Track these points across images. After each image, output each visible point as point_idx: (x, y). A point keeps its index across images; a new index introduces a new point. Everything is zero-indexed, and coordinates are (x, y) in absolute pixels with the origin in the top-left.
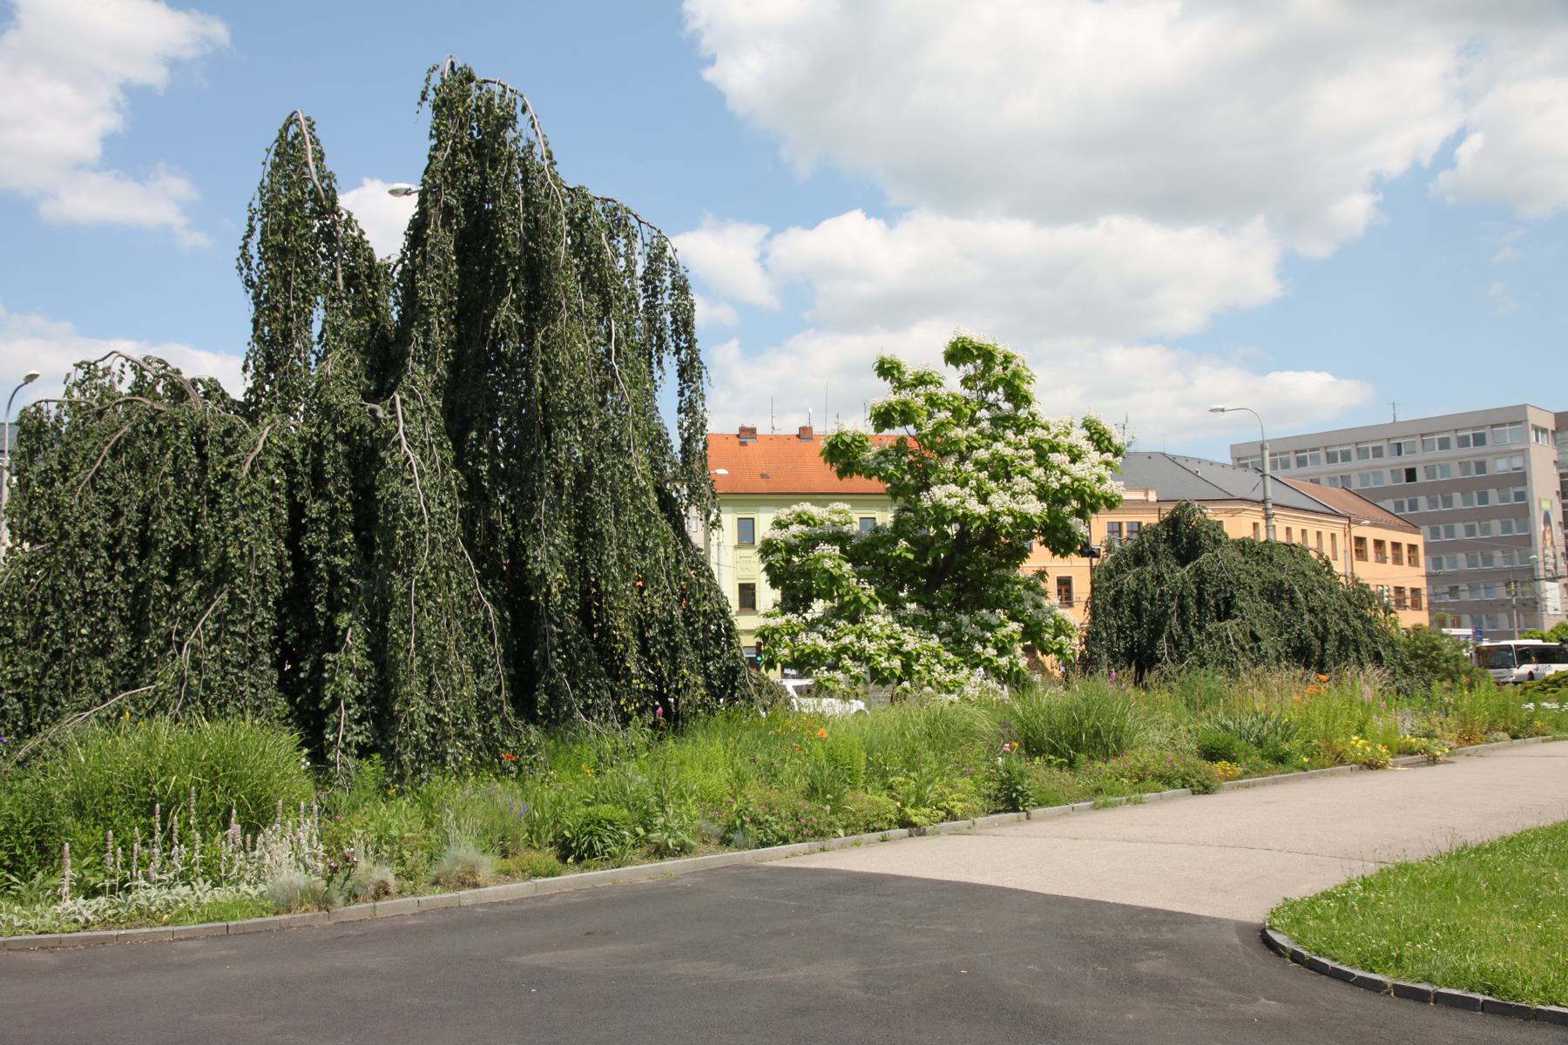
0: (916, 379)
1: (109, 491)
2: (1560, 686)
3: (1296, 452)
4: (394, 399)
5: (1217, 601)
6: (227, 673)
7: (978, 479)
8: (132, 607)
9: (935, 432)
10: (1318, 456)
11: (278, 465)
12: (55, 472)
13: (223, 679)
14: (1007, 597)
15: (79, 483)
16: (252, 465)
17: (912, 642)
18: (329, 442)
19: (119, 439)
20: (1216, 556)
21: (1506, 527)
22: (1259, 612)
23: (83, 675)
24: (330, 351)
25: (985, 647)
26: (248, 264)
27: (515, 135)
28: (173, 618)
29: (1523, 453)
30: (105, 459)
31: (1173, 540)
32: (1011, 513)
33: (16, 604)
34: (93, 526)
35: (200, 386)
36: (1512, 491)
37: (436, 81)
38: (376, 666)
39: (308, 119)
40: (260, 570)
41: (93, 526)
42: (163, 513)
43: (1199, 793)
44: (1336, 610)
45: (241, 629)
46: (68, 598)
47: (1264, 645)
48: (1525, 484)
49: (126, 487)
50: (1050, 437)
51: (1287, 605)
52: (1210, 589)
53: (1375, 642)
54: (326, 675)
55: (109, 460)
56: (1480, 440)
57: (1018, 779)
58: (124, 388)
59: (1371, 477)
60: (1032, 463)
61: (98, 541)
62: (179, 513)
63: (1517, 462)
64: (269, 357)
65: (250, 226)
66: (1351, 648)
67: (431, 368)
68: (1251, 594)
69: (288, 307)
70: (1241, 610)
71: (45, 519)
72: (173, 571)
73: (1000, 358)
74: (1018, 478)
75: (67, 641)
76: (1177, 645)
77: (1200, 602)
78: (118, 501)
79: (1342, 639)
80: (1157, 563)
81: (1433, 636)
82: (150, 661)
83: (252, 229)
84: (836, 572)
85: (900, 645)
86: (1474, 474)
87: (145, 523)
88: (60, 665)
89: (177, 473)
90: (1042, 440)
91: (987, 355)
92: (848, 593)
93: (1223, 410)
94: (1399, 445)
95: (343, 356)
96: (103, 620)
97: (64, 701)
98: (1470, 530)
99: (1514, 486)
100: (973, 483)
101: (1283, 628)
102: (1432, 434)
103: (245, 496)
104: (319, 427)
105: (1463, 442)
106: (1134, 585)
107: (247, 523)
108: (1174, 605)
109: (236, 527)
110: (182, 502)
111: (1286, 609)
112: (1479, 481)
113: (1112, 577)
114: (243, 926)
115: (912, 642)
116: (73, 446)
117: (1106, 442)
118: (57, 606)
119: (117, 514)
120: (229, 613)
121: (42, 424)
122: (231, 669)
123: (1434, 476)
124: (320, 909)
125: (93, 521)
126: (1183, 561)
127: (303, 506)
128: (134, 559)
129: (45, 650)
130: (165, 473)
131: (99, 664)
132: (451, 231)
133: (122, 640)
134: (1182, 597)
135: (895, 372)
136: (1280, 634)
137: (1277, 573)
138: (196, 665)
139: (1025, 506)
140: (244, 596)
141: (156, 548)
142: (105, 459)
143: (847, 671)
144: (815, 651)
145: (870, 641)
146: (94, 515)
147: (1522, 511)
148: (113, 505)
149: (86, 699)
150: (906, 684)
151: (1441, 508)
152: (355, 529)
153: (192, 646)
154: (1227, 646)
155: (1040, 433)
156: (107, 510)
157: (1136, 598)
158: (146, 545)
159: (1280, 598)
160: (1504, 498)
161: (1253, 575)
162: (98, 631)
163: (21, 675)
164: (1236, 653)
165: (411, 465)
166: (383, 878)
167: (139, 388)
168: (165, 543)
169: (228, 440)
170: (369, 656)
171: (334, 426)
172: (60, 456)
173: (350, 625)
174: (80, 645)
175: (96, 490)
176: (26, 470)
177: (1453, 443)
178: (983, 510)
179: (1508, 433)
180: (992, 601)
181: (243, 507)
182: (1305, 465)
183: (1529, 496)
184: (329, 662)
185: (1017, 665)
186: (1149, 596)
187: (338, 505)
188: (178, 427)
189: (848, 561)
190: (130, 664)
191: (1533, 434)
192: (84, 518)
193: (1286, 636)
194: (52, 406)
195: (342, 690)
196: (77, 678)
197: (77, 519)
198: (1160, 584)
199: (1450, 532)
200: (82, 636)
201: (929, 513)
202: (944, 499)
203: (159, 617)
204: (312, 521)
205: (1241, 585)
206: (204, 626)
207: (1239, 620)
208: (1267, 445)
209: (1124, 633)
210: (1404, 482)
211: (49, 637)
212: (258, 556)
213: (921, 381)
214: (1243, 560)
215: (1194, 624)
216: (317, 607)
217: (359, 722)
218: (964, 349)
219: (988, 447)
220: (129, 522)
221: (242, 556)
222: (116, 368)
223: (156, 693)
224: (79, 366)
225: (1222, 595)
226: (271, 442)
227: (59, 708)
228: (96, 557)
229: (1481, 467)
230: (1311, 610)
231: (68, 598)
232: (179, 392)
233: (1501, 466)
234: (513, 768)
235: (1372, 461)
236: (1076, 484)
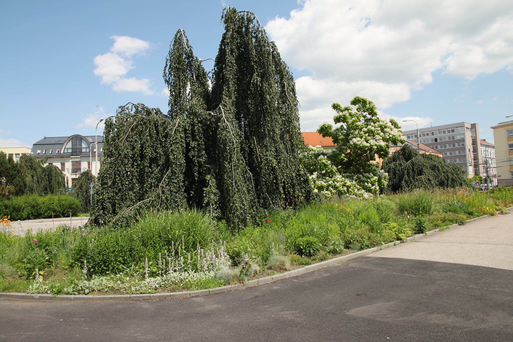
0: (345, 109)
1: (131, 142)
3: (407, 135)
4: (220, 107)
6: (172, 195)
7: (365, 136)
8: (139, 175)
9: (353, 123)
10: (413, 136)
11: (182, 131)
12: (116, 137)
13: (171, 197)
14: (371, 170)
15: (123, 139)
16: (175, 132)
17: (348, 183)
18: (196, 123)
19: (133, 126)
20: (417, 158)
22: (430, 173)
23: (127, 196)
24: (193, 98)
25: (368, 184)
26: (166, 75)
27: (253, 26)
28: (152, 178)
29: (464, 134)
30: (129, 132)
31: (404, 154)
32: (376, 145)
33: (108, 175)
34: (128, 152)
35: (154, 110)
36: (461, 144)
37: (225, 12)
38: (220, 191)
39: (183, 31)
40: (180, 163)
41: (128, 152)
42: (147, 147)
43: (461, 225)
45: (175, 181)
46: (122, 173)
49: (136, 140)
50: (384, 124)
52: (415, 167)
54: (204, 195)
55: (131, 132)
56: (453, 131)
57: (423, 223)
58: (132, 113)
59: (426, 141)
60: (380, 131)
61: (129, 156)
62: (151, 147)
63: (462, 136)
64: (175, 101)
65: (166, 64)
66: (455, 182)
67: (230, 98)
68: (427, 168)
69: (180, 85)
70: (425, 173)
71: (114, 151)
72: (151, 165)
73: (368, 103)
74: (377, 136)
75: (122, 186)
77: (413, 170)
78: (134, 144)
79: (453, 180)
80: (400, 161)
82: (146, 192)
83: (167, 65)
84: (326, 163)
85: (346, 183)
86: (452, 140)
87: (142, 150)
88: (121, 193)
89: (150, 135)
90: (382, 125)
91: (364, 102)
92: (329, 169)
93: (406, 121)
94: (433, 133)
95: (197, 99)
96: (132, 179)
97: (122, 204)
98: (451, 154)
99: (461, 142)
100: (364, 137)
101: (436, 177)
102: (441, 130)
103: (174, 140)
104: (193, 119)
105: (449, 132)
106: (393, 166)
107: (175, 148)
108: (406, 172)
109: (172, 149)
110: (152, 144)
111: (437, 172)
112: (453, 141)
113: (387, 165)
114: (215, 291)
115: (348, 183)
116: (120, 129)
117: (397, 126)
118: (119, 176)
119: (134, 148)
120: (172, 176)
121: (111, 123)
122: (173, 194)
123: (442, 140)
124: (240, 283)
125: (127, 150)
126: (407, 160)
127: (189, 143)
128: (139, 161)
129: (116, 189)
130: (147, 135)
131: (131, 193)
132: (233, 57)
133: (137, 185)
134: (408, 170)
135: (338, 107)
136: (436, 179)
137: (434, 162)
138: (163, 192)
139: (380, 143)
140: (176, 171)
141: (146, 158)
142: (129, 132)
143: (331, 191)
144: (322, 186)
145: (337, 183)
146: (128, 149)
147: (464, 149)
148: (132, 145)
149: (129, 203)
150: (348, 195)
151: (443, 148)
152: (205, 150)
153: (162, 187)
155: (381, 123)
156: (131, 147)
157: (394, 170)
158: (142, 156)
160: (459, 145)
161: (428, 163)
162: (130, 183)
163: (110, 196)
164: (425, 184)
165: (228, 127)
166: (255, 269)
167: (137, 112)
168: (148, 156)
169: (164, 125)
170: (217, 189)
171: (197, 119)
172: (117, 132)
173: (210, 179)
174: (126, 187)
175: (127, 141)
176: (108, 137)
177: (446, 132)
178: (368, 145)
179: (460, 130)
180: (368, 171)
181: (173, 143)
183: (465, 145)
184: (205, 191)
185: (376, 189)
187: (200, 142)
188: (150, 122)
189: (329, 161)
190: (140, 192)
191: (466, 129)
192: (125, 149)
193: (437, 179)
194: (114, 118)
195: (210, 199)
196: (126, 197)
197: (123, 150)
198: (401, 166)
200: (127, 184)
201: (352, 146)
202: (357, 142)
203: (148, 178)
204: (192, 147)
205: (424, 166)
206: (164, 180)
208: (418, 130)
209: (391, 180)
210: (434, 142)
211: (117, 185)
212: (179, 158)
213: (347, 109)
214: (424, 159)
216: (195, 174)
217: (216, 210)
218: (358, 100)
219: (366, 127)
220: (137, 150)
221: (174, 159)
222: (130, 108)
223: (150, 201)
224: (120, 107)
225: (419, 169)
226: (180, 123)
227: (121, 206)
228: (129, 161)
229: (453, 138)
230: (444, 172)
231: (122, 173)
232: (149, 113)
233: (458, 137)
234: (260, 223)
235: (426, 137)
236: (394, 137)
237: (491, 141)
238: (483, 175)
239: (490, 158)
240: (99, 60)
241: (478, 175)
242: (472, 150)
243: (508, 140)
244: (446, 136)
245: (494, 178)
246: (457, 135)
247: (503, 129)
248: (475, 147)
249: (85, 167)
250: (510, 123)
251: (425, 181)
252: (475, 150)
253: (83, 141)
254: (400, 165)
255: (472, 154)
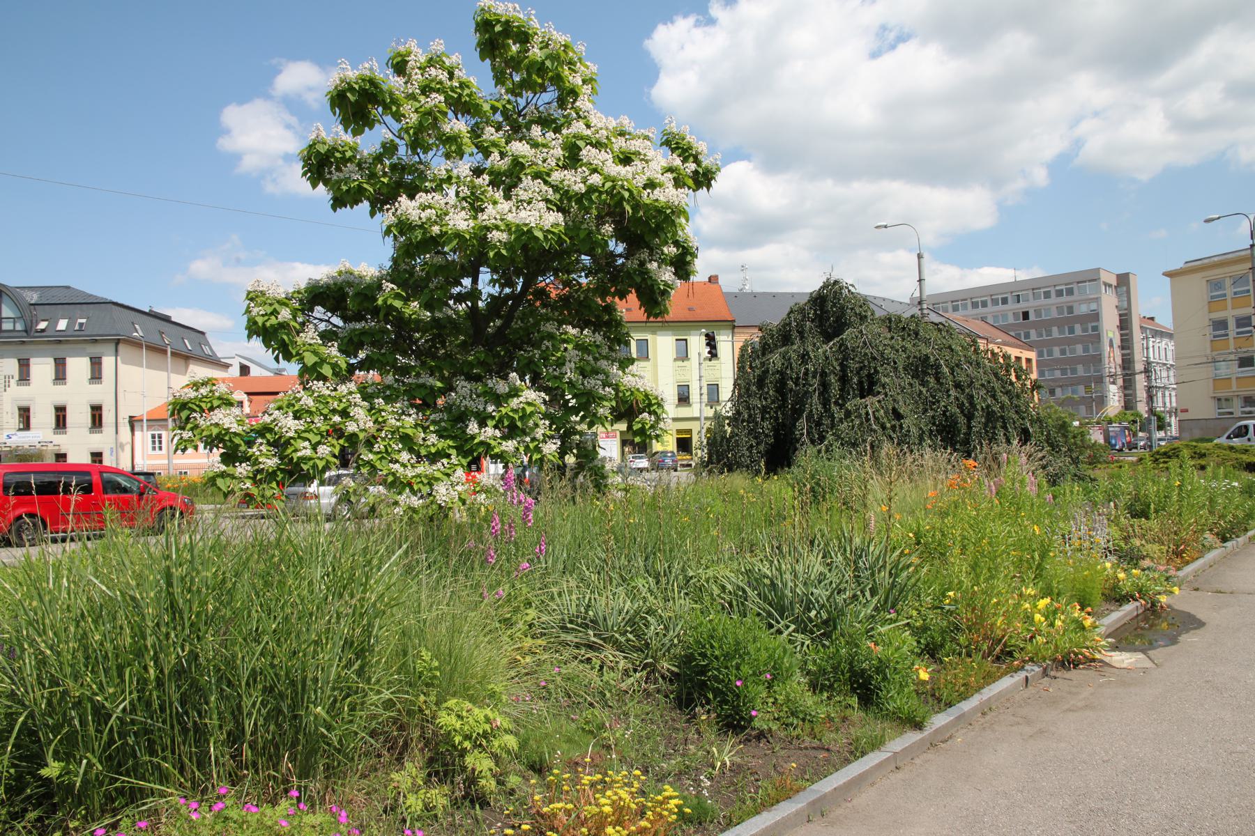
2: (1169, 457)
5: (861, 378)
21: (1086, 349)
29: (1097, 300)
31: (820, 319)
36: (1090, 326)
44: (983, 385)
47: (906, 423)
48: (1098, 320)
51: (932, 380)
52: (853, 365)
53: (1023, 419)
56: (1070, 292)
63: (1094, 306)
66: (999, 424)
68: (896, 369)
76: (819, 424)
77: (844, 379)
79: (990, 415)
81: (1063, 415)
93: (886, 227)
98: (1063, 352)
108: (816, 383)
112: (1069, 320)
126: (828, 338)
136: (925, 411)
137: (922, 347)
147: (1096, 337)
154: (865, 425)
159: (925, 373)
160: (1085, 330)
161: (899, 350)
164: (875, 431)
177: (1053, 294)
182: (958, 310)
186: (794, 376)
191: (1103, 287)
193: (930, 413)
199: (1050, 353)
205: (885, 360)
207: (881, 397)
215: (836, 403)
229: (1070, 310)
230: (958, 386)
233: (1083, 309)
235: (1001, 307)
237: (1165, 320)
238: (1142, 408)
239: (1165, 364)
240: (232, 115)
241: (1131, 408)
242: (1117, 342)
243: (1209, 308)
244: (1051, 307)
245: (1173, 418)
246: (1081, 302)
247: (1199, 275)
248: (1126, 335)
249: (11, 373)
250: (1216, 259)
251: (876, 419)
252: (1126, 343)
253: (5, 298)
254: (803, 356)
255: (1118, 353)
